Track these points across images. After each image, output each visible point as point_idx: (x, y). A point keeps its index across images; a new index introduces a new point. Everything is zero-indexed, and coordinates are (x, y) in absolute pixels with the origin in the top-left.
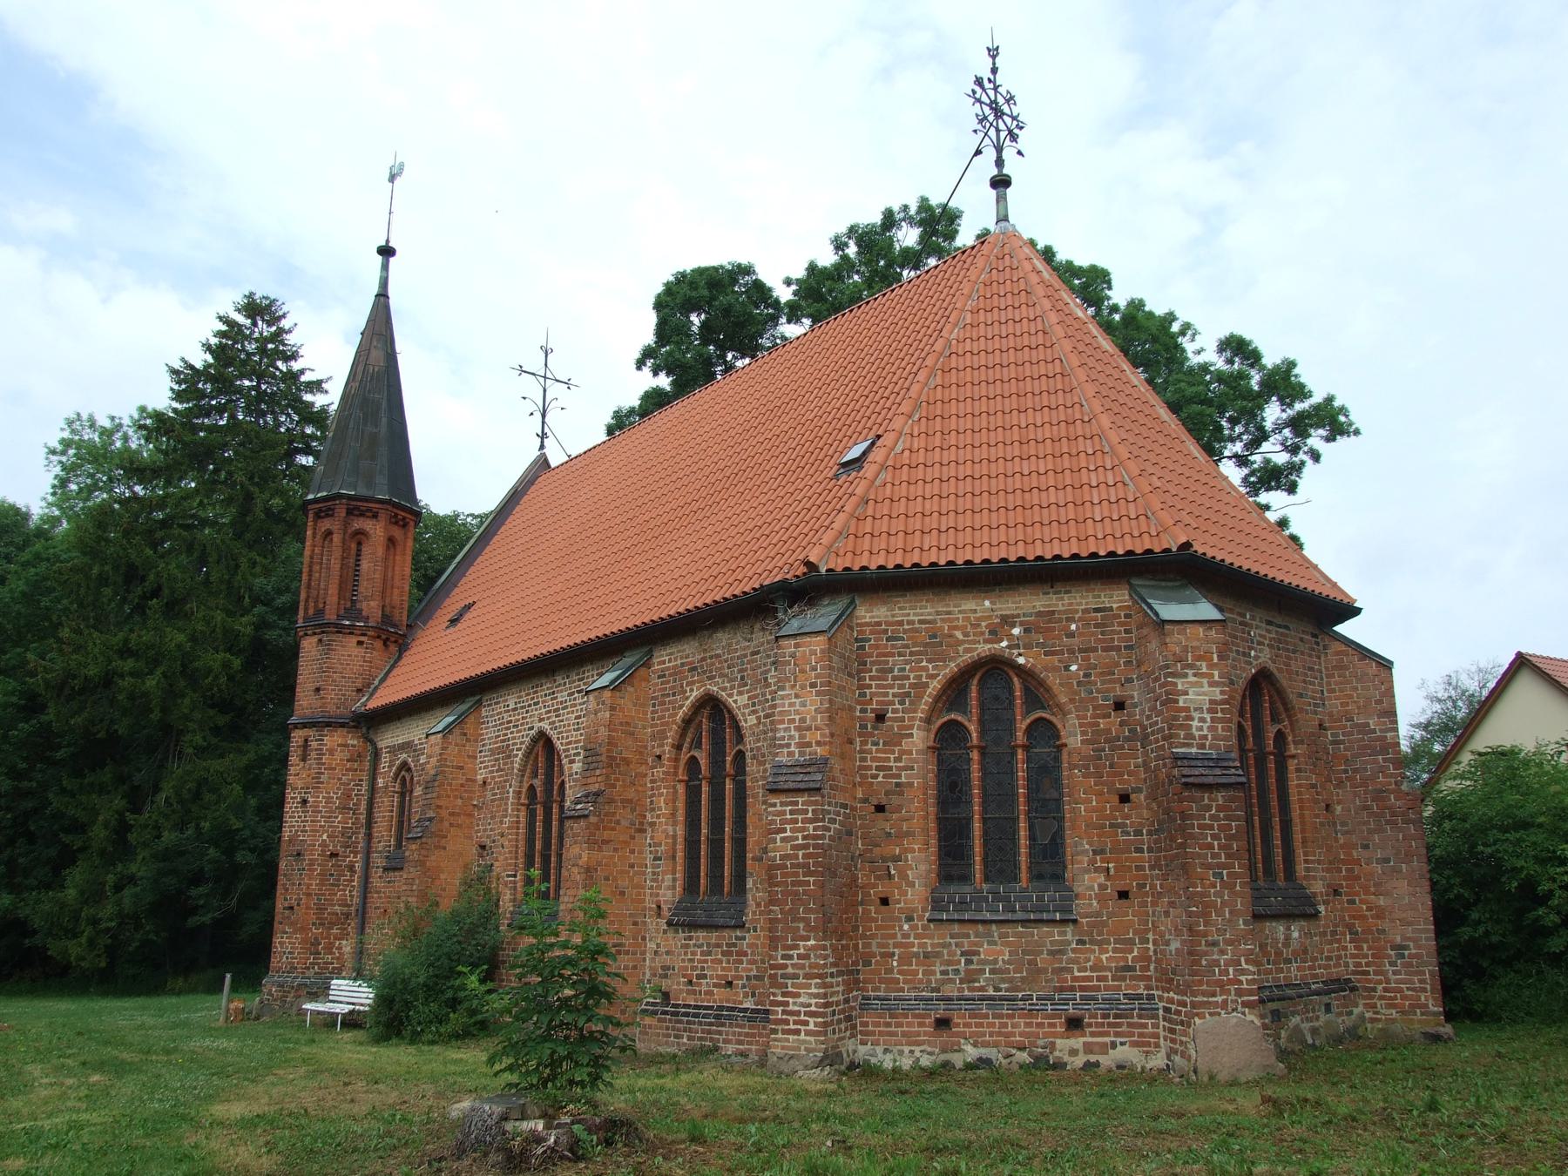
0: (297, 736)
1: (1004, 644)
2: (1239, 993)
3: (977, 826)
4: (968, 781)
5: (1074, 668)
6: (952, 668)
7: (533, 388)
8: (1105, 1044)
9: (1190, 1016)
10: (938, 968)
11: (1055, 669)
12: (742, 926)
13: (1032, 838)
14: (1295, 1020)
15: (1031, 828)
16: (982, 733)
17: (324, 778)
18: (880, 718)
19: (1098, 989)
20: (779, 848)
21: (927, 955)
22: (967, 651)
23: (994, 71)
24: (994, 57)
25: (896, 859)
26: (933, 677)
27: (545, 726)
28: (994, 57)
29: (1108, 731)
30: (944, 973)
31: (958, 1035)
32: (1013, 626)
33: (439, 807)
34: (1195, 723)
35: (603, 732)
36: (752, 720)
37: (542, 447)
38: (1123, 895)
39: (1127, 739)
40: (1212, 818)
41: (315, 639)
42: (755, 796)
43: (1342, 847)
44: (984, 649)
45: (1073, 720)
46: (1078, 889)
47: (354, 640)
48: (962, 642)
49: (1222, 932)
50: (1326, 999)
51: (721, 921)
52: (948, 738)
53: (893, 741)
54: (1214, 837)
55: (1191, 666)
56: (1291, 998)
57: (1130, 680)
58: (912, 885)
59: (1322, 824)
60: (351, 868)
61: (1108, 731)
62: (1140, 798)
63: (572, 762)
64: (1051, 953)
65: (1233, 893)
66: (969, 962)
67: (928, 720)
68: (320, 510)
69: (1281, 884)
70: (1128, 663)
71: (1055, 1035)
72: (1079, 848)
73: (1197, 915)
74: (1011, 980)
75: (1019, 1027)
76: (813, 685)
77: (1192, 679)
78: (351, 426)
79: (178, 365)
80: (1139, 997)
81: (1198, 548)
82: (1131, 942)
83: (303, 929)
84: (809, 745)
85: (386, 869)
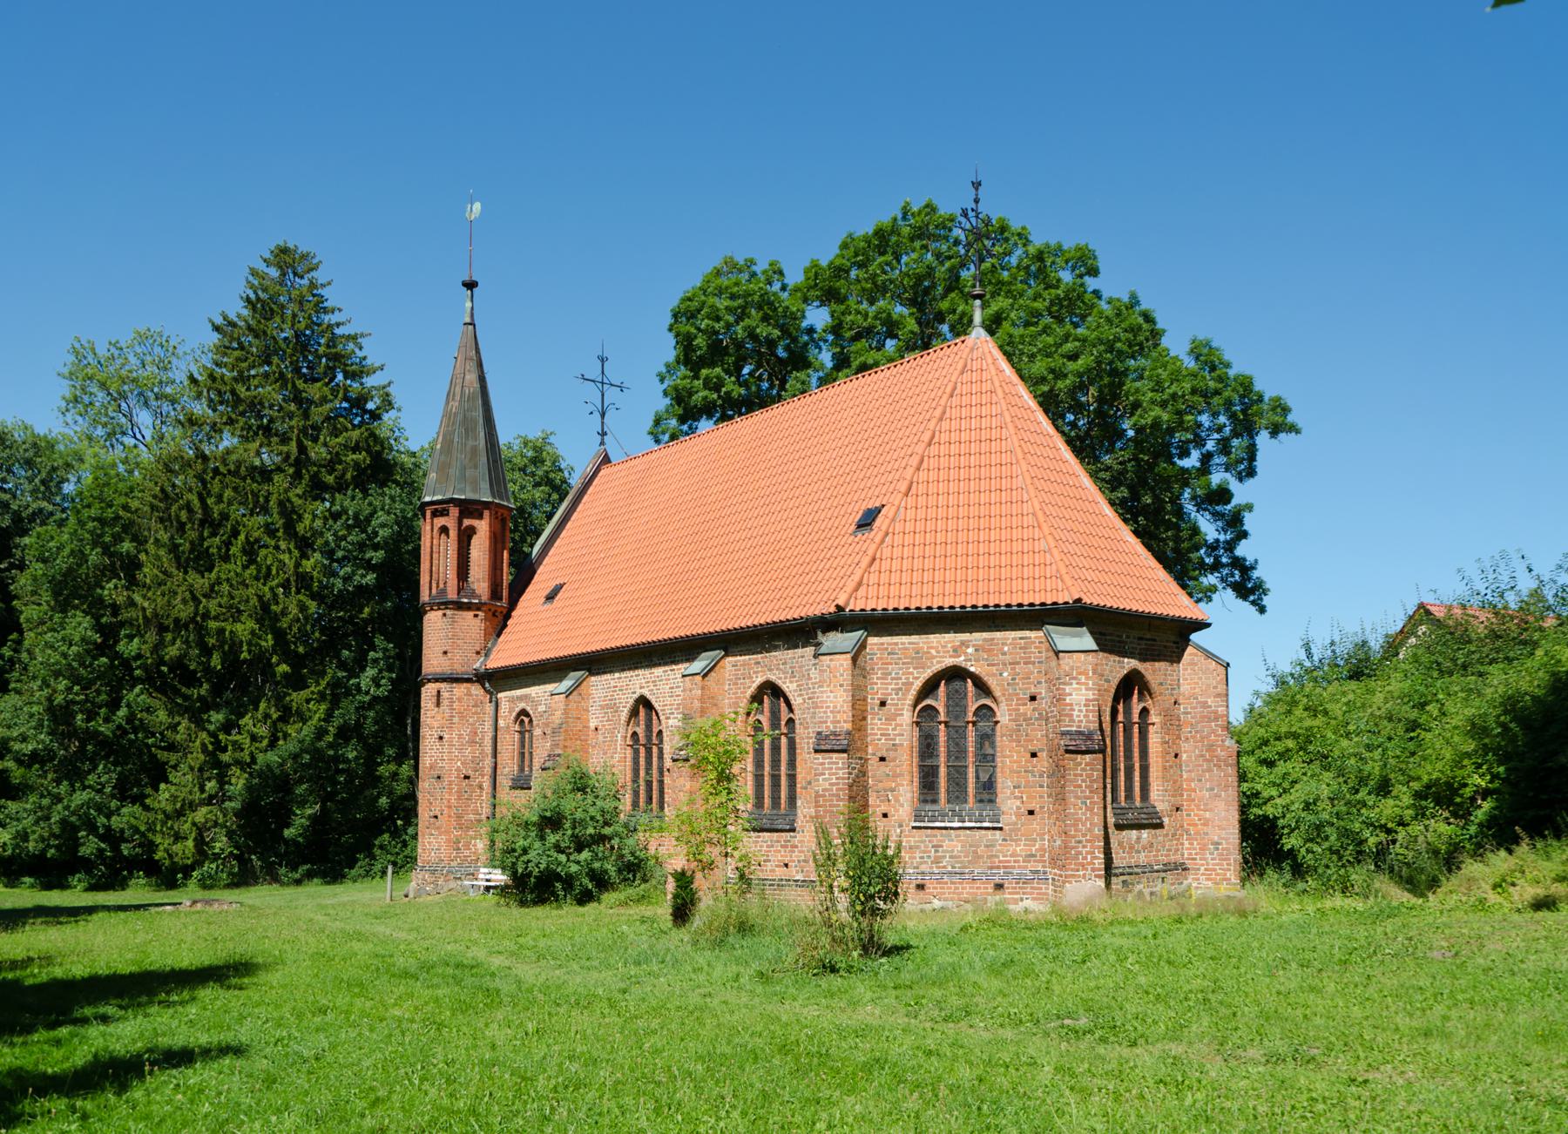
0: (428, 691)
1: (962, 658)
2: (1093, 870)
3: (943, 771)
4: (937, 743)
5: (1005, 674)
6: (928, 673)
7: (592, 392)
8: (1016, 899)
9: (1064, 882)
10: (918, 855)
11: (994, 675)
12: (793, 830)
13: (977, 777)
14: (1139, 887)
15: (977, 771)
16: (948, 713)
17: (456, 720)
18: (883, 704)
19: (1014, 867)
20: (822, 784)
21: (911, 848)
22: (938, 662)
23: (977, 201)
24: (977, 189)
25: (893, 790)
26: (917, 678)
27: (646, 692)
28: (977, 189)
29: (1026, 714)
30: (922, 858)
31: (929, 894)
32: (968, 647)
33: (565, 747)
34: (1076, 713)
35: (697, 704)
36: (800, 700)
37: (602, 443)
38: (1031, 813)
39: (1037, 719)
40: (1082, 770)
41: (440, 613)
42: (802, 748)
43: (1186, 780)
44: (949, 662)
45: (1003, 706)
46: (1004, 808)
47: (471, 614)
48: (934, 657)
49: (1084, 835)
50: (1163, 875)
51: (780, 827)
52: (926, 715)
53: (891, 718)
54: (1083, 781)
55: (1075, 678)
56: (1137, 874)
57: (1039, 683)
58: (902, 806)
59: (1171, 767)
60: (481, 787)
61: (1026, 714)
62: (1043, 755)
63: (668, 718)
64: (987, 846)
65: (1093, 814)
66: (936, 851)
67: (915, 706)
68: (436, 510)
69: (1138, 803)
70: (1040, 672)
71: (988, 894)
72: (1004, 784)
73: (1071, 825)
74: (961, 862)
75: (967, 890)
76: (841, 686)
77: (1075, 686)
78: (456, 440)
79: (219, 321)
80: (1037, 872)
81: (1087, 600)
82: (1035, 840)
83: (447, 832)
84: (839, 722)
85: (512, 788)
